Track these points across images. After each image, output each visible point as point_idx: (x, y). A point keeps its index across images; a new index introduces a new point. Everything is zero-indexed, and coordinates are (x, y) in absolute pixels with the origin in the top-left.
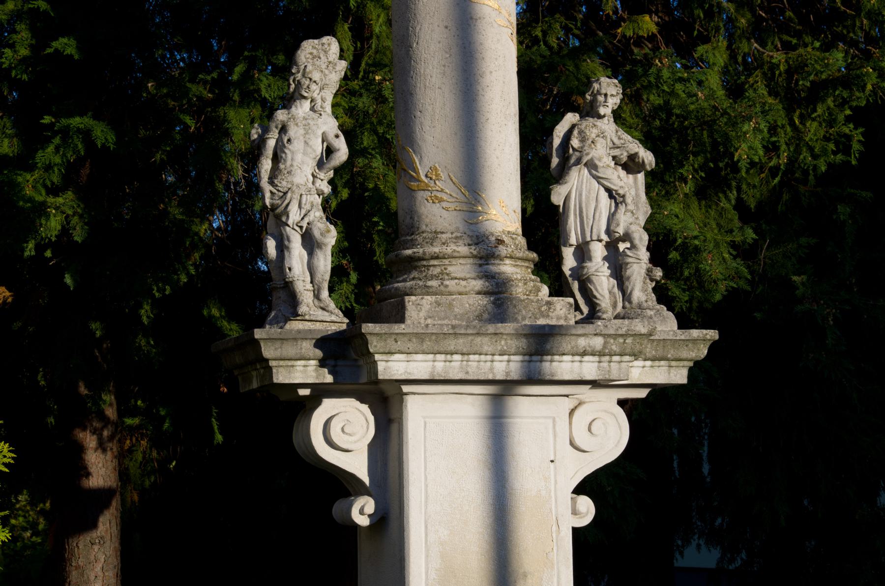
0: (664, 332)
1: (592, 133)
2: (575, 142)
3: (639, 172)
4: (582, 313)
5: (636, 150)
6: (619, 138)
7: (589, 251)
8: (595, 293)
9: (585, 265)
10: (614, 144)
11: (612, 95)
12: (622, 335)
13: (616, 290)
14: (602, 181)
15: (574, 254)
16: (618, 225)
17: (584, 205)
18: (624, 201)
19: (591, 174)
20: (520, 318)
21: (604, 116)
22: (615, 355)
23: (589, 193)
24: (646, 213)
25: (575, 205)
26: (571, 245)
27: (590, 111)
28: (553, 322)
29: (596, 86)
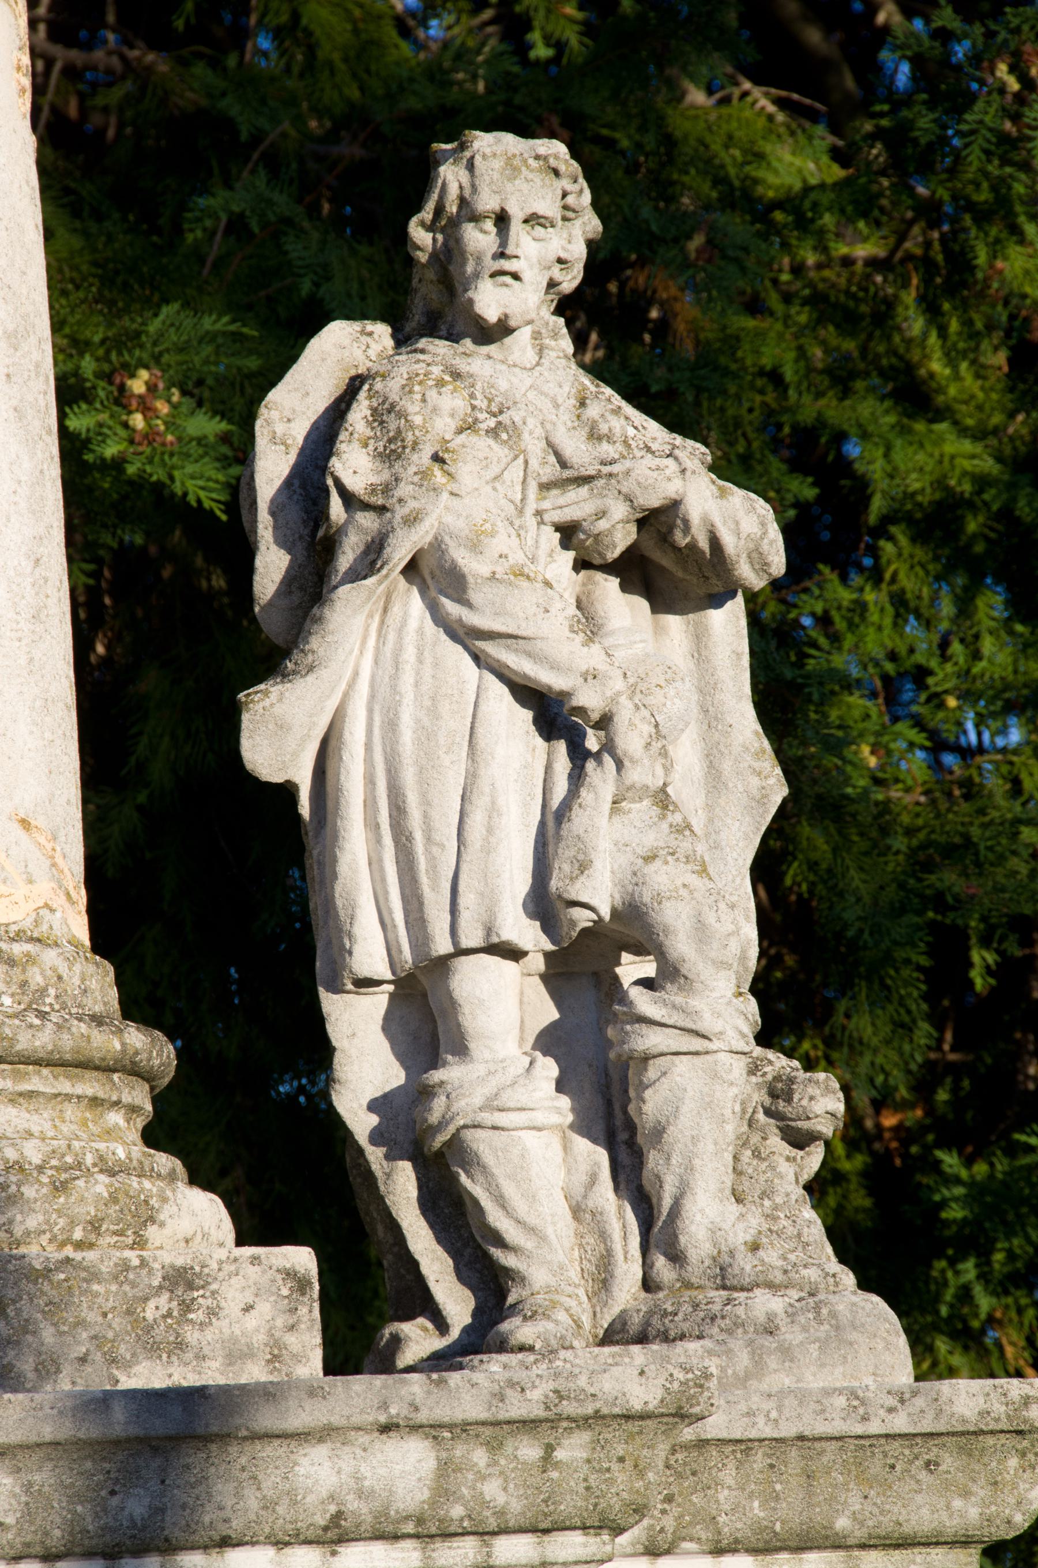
0: (802, 1396)
1: (436, 413)
2: (354, 466)
3: (717, 600)
4: (441, 1325)
5: (672, 489)
6: (595, 436)
7: (452, 1006)
8: (496, 1218)
9: (436, 1076)
10: (563, 464)
11: (532, 220)
12: (528, 1425)
13: (606, 1196)
14: (491, 649)
15: (388, 1025)
16: (583, 867)
17: (409, 778)
18: (608, 746)
19: (439, 618)
20: (26, 1366)
21: (502, 330)
22: (504, 1531)
23: (434, 712)
24: (762, 801)
25: (370, 781)
26: (365, 983)
27: (428, 305)
28: (212, 1374)
29: (451, 176)
